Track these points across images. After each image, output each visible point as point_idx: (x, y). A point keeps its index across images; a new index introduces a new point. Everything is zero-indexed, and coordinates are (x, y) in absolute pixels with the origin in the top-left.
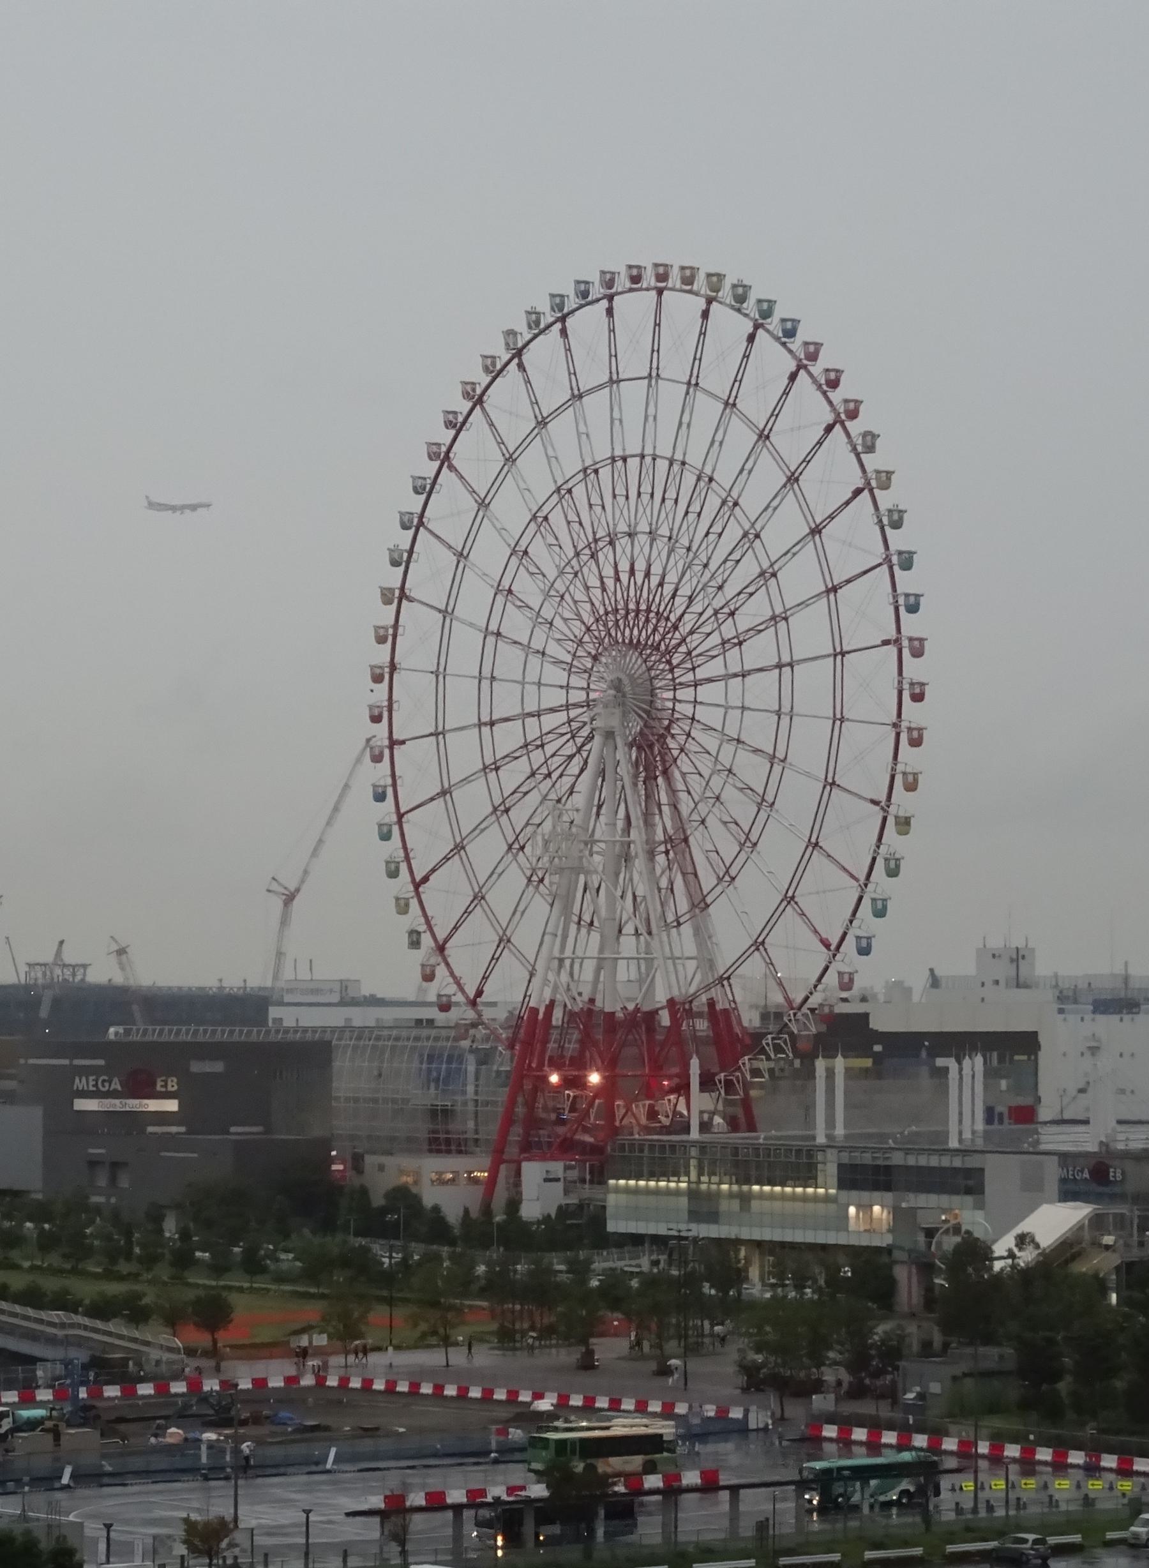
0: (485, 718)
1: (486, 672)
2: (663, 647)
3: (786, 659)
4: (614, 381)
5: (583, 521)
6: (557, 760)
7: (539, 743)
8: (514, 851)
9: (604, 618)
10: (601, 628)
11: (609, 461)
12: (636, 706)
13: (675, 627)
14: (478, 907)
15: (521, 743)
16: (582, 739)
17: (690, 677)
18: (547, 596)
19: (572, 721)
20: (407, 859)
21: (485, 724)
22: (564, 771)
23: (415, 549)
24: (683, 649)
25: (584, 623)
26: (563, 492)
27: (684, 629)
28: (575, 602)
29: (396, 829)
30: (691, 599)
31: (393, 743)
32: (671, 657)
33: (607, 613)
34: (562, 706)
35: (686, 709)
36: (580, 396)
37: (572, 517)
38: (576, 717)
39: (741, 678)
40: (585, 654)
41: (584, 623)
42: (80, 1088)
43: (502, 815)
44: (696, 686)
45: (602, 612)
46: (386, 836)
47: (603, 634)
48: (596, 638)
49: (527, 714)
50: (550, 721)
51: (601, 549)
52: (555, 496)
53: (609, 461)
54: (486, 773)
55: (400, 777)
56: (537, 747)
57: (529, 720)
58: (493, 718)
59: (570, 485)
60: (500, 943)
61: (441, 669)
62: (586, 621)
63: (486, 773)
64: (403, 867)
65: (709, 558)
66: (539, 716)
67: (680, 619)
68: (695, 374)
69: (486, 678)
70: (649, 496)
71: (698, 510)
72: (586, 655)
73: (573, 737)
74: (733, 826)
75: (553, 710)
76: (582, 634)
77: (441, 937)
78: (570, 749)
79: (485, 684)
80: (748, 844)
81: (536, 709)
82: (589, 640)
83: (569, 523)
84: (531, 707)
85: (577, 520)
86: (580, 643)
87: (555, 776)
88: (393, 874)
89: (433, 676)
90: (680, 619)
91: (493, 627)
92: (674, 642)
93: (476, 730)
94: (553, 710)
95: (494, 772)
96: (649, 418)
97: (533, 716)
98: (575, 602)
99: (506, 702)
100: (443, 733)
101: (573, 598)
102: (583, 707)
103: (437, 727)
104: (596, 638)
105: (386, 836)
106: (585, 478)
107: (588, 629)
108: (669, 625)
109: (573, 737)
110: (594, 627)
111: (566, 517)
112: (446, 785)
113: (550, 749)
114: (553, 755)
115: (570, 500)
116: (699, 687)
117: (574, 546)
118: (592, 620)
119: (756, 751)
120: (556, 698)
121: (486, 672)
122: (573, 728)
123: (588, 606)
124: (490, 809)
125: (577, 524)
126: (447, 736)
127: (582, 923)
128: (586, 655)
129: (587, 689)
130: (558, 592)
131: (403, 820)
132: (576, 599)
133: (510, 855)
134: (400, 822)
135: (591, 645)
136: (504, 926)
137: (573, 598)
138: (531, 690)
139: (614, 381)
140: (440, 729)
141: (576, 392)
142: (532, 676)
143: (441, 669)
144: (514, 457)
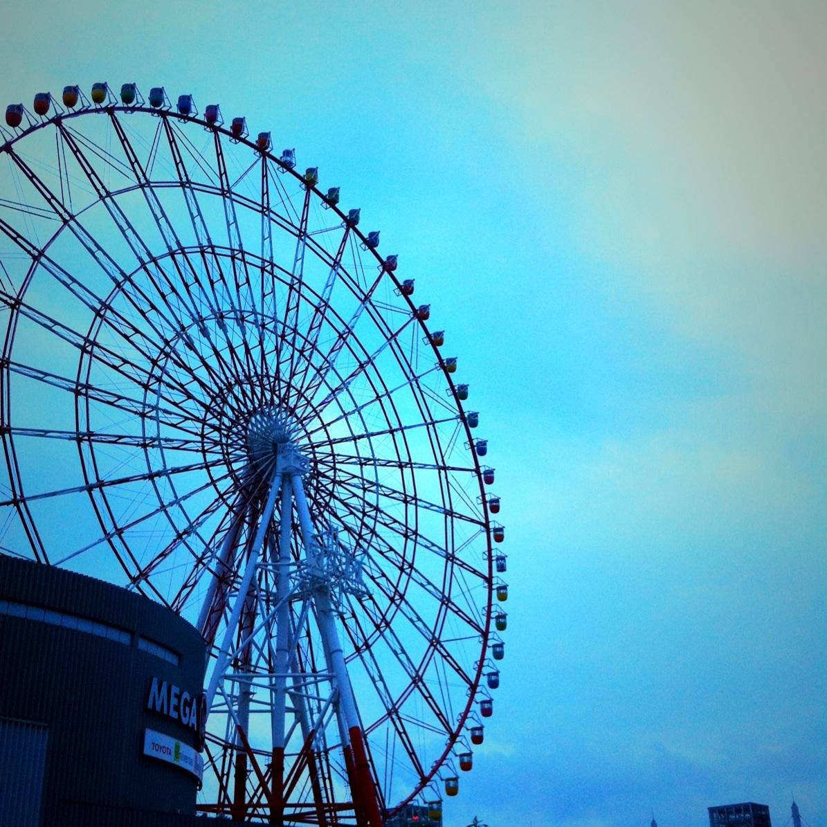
1: (110, 528)
2: (277, 401)
5: (371, 580)
6: (302, 367)
7: (322, 372)
9: (322, 509)
10: (321, 501)
11: (370, 642)
13: (277, 378)
16: (291, 394)
22: (292, 362)
24: (293, 392)
27: (285, 375)
28: (352, 513)
30: (278, 351)
32: (287, 404)
33: (321, 514)
37: (382, 581)
38: (306, 407)
40: (327, 474)
42: (158, 708)
43: (320, 304)
44: (221, 496)
45: (326, 514)
47: (318, 497)
48: (323, 491)
50: (323, 392)
54: (347, 327)
56: (321, 368)
61: (414, 383)
62: (336, 501)
66: (333, 392)
73: (299, 392)
76: (335, 490)
78: (297, 381)
83: (384, 575)
85: (377, 580)
87: (297, 354)
91: (398, 435)
92: (283, 391)
97: (337, 389)
99: (361, 389)
101: (355, 515)
104: (323, 491)
106: (384, 616)
108: (272, 379)
110: (327, 499)
111: (387, 579)
113: (312, 372)
114: (307, 369)
115: (375, 619)
118: (331, 504)
120: (330, 413)
121: (385, 400)
122: (303, 399)
123: (340, 514)
125: (375, 577)
128: (326, 474)
135: (324, 483)
137: (355, 515)
138: (349, 407)
143: (414, 383)
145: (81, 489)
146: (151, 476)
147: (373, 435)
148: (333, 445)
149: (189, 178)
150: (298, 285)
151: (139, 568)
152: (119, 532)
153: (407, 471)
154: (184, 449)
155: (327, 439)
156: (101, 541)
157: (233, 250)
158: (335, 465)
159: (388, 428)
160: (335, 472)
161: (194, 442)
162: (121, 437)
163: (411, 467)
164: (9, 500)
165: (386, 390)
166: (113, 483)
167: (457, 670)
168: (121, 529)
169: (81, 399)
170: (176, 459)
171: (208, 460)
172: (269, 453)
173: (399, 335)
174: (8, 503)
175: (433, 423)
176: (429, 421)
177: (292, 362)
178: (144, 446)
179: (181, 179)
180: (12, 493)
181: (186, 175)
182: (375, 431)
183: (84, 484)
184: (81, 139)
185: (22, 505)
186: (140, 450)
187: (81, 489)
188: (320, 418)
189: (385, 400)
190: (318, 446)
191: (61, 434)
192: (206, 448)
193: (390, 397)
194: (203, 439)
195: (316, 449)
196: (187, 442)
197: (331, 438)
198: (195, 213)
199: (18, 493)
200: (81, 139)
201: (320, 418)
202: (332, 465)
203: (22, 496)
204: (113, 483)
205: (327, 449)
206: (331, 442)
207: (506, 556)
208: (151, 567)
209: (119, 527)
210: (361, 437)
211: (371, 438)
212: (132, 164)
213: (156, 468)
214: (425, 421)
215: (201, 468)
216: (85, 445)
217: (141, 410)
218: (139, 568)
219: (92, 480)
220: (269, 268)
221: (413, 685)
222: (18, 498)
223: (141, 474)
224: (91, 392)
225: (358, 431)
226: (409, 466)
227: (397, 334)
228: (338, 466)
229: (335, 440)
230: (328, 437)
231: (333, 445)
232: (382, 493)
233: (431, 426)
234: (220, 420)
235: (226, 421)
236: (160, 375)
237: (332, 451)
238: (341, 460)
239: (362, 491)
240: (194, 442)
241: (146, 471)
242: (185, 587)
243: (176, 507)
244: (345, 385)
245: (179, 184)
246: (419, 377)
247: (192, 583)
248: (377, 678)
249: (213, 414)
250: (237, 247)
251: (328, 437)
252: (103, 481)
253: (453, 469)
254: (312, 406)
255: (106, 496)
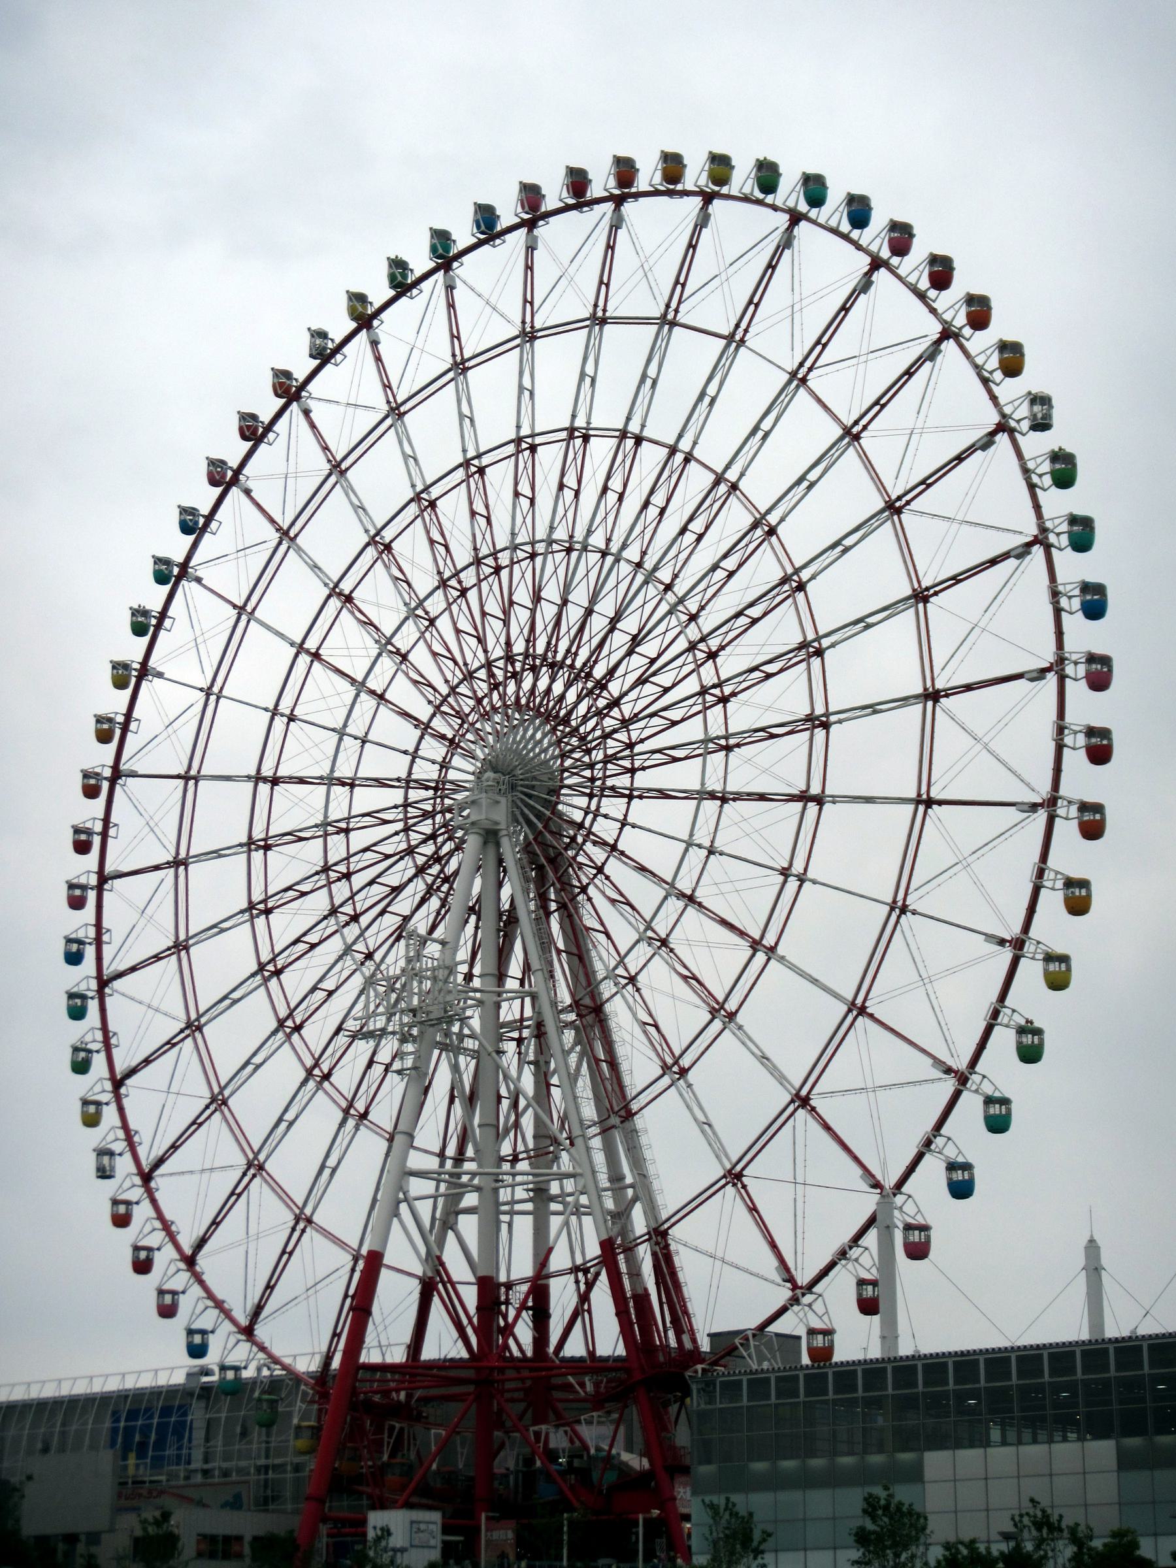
0: (267, 771)
3: (815, 790)
4: (599, 320)
7: (343, 825)
8: (266, 974)
12: (522, 800)
14: (190, 1040)
15: (319, 819)
17: (623, 781)
18: (411, 614)
19: (409, 805)
20: (99, 942)
21: (265, 780)
22: (388, 905)
23: (217, 517)
25: (485, 651)
26: (524, 446)
28: (484, 614)
29: (92, 896)
31: (117, 774)
34: (398, 780)
35: (605, 829)
36: (603, 321)
38: (416, 802)
39: (718, 803)
41: (485, 651)
44: (630, 797)
46: (77, 903)
49: (338, 779)
50: (368, 799)
51: (519, 562)
52: (461, 471)
53: (564, 435)
55: (116, 825)
57: (337, 790)
58: (279, 774)
59: (485, 460)
60: (211, 1103)
61: (216, 689)
63: (250, 850)
64: (90, 952)
65: (702, 608)
66: (352, 786)
67: (423, 901)
68: (744, 325)
69: (282, 715)
70: (617, 496)
71: (700, 530)
72: (470, 694)
73: (407, 829)
74: (652, 1030)
75: (380, 783)
77: (120, 1067)
79: (279, 722)
80: (675, 1069)
81: (350, 774)
82: (484, 677)
84: (344, 770)
86: (469, 676)
88: (74, 958)
89: (201, 696)
90: (423, 901)
91: (311, 644)
93: (250, 786)
94: (380, 783)
95: (261, 852)
96: (647, 381)
97: (343, 784)
98: (484, 614)
100: (196, 779)
102: (427, 788)
103: (190, 767)
105: (77, 903)
107: (489, 665)
109: (407, 829)
112: (183, 855)
116: (635, 801)
117: (475, 549)
119: (690, 978)
121: (285, 707)
124: (245, 905)
126: (201, 783)
127: (352, 1111)
129: (444, 765)
130: (427, 613)
131: (106, 886)
132: (487, 609)
133: (259, 977)
134: (100, 889)
136: (223, 1083)
137: (482, 606)
139: (599, 320)
140: (193, 772)
141: (600, 314)
142: (356, 727)
144: (402, 409)
145: (782, 959)
146: (691, 899)
147: (353, 681)
148: (425, 720)
149: (292, 1223)
150: (268, 968)
151: (804, 808)
152: (785, 873)
153: (346, 587)
154: (622, 895)
155: (426, 737)
156: (266, 709)
157: (288, 1037)
158: (448, 695)
159: (316, 664)
160: (457, 686)
161: (603, 893)
162: (685, 978)
163: (336, 585)
164: (867, 1021)
165: (272, 719)
166: (742, 934)
167: (532, 269)
168: (782, 874)
169: (685, 1062)
170: (645, 895)
171: (606, 855)
172: (522, 786)
173: (175, 773)
174: (871, 1016)
175: (241, 609)
176: (244, 618)
177: (388, 905)
178: (664, 942)
179: (254, 1176)
180: (856, 1024)
181: (244, 1174)
182: (345, 685)
183: (772, 962)
184: (196, 1225)
185: (859, 1001)
186: (673, 942)
187: (782, 959)
188: (410, 773)
189: (285, 707)
190: (443, 737)
191: (746, 1039)
192: (594, 871)
193: (277, 705)
194: (588, 884)
195: (450, 736)
196: (613, 901)
197: (418, 733)
198: (327, 1172)
199: (850, 1018)
200: (196, 1225)
201: (410, 773)
202: (451, 700)
203: (850, 1011)
204: (742, 934)
205: (438, 724)
206: (425, 728)
207: (309, 329)
208: (792, 798)
209: (782, 878)
210: (372, 692)
211: (360, 678)
212: (239, 1195)
213: (675, 905)
214: (248, 622)
215: (622, 853)
216: (731, 1006)
217: (630, 987)
218: (804, 808)
219: (761, 957)
220: (289, 1023)
221: (617, 434)
222: (855, 1013)
223: (700, 914)
224: (669, 1061)
225: (367, 703)
226: (337, 590)
227: (178, 777)
228: (444, 690)
229: (416, 726)
230: (422, 738)
231: (425, 720)
232: (437, 695)
233: (249, 608)
234: (506, 678)
235: (511, 687)
236: (503, 565)
237: (433, 715)
238: (429, 689)
239: (438, 623)
240: (603, 893)
241: (691, 911)
242: (773, 736)
243: (697, 839)
244: (330, 781)
245: (264, 1173)
246: (201, 690)
247: (761, 734)
248: (649, 382)
249: (506, 666)
250: (280, 1035)
251: (422, 738)
252: (751, 947)
253: (272, 521)
254: (406, 798)
255: (762, 927)
